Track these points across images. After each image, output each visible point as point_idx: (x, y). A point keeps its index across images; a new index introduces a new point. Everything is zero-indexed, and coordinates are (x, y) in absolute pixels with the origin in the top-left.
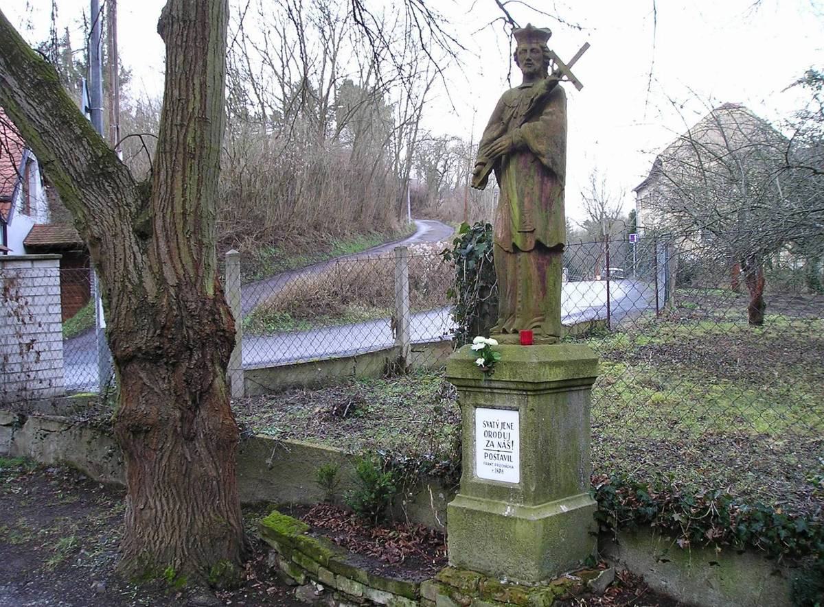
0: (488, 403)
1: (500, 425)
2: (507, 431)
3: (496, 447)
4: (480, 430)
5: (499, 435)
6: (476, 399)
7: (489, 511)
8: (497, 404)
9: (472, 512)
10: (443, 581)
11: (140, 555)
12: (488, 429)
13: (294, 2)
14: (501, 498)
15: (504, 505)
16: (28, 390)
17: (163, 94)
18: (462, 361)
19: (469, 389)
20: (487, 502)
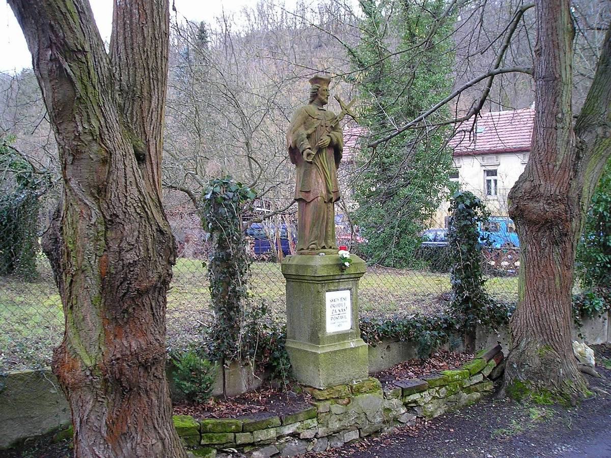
0: (336, 288)
1: (339, 299)
2: (344, 301)
3: (338, 312)
4: (328, 304)
5: (339, 305)
6: (328, 286)
7: (344, 348)
8: (341, 288)
9: (335, 352)
10: (328, 398)
11: (342, 452)
12: (333, 303)
13: (74, 2)
14: (344, 340)
15: (348, 342)
16: (22, 336)
17: (512, 185)
18: (327, 265)
19: (326, 282)
20: (339, 344)
